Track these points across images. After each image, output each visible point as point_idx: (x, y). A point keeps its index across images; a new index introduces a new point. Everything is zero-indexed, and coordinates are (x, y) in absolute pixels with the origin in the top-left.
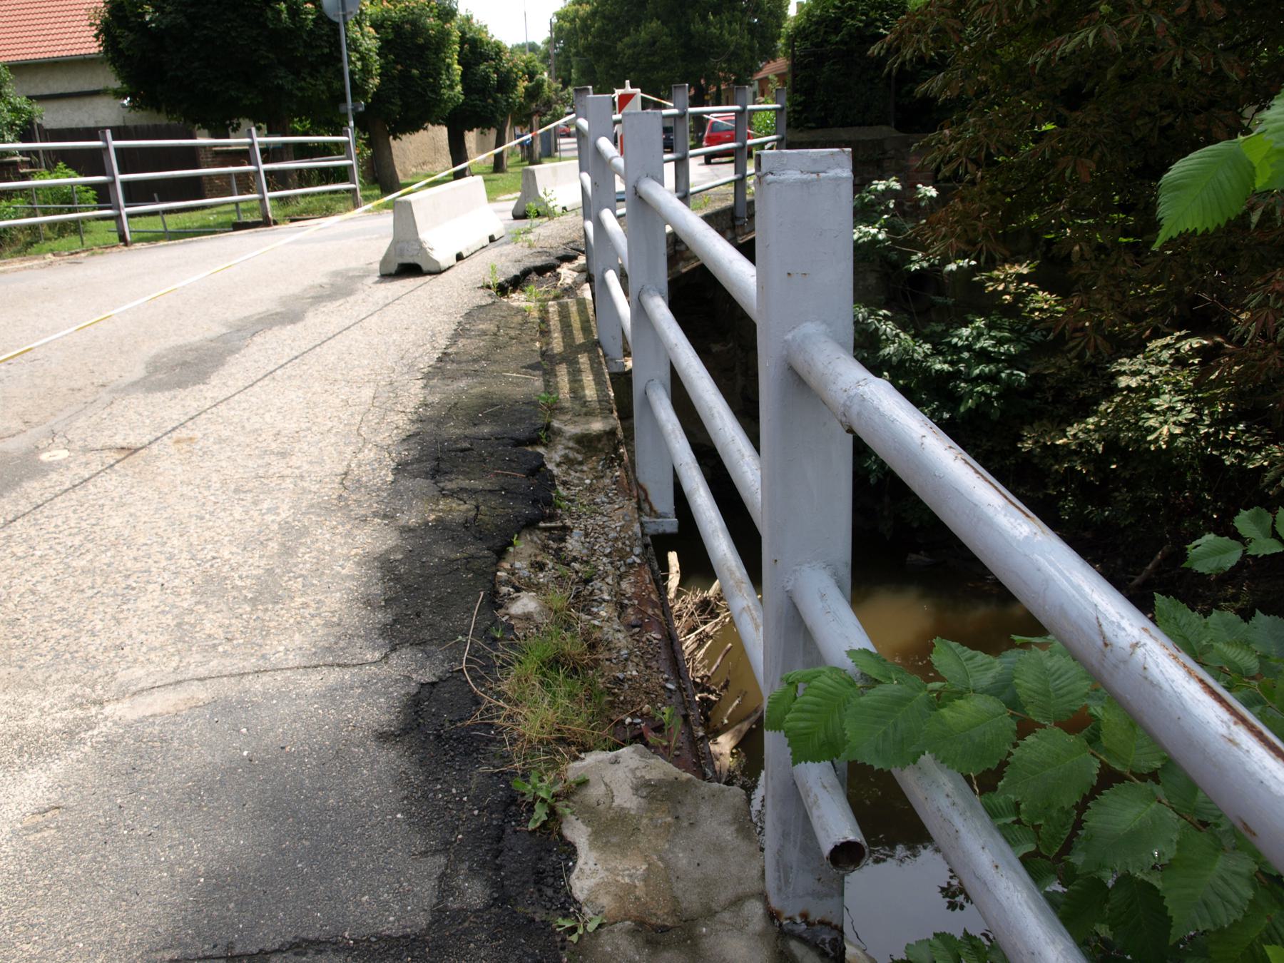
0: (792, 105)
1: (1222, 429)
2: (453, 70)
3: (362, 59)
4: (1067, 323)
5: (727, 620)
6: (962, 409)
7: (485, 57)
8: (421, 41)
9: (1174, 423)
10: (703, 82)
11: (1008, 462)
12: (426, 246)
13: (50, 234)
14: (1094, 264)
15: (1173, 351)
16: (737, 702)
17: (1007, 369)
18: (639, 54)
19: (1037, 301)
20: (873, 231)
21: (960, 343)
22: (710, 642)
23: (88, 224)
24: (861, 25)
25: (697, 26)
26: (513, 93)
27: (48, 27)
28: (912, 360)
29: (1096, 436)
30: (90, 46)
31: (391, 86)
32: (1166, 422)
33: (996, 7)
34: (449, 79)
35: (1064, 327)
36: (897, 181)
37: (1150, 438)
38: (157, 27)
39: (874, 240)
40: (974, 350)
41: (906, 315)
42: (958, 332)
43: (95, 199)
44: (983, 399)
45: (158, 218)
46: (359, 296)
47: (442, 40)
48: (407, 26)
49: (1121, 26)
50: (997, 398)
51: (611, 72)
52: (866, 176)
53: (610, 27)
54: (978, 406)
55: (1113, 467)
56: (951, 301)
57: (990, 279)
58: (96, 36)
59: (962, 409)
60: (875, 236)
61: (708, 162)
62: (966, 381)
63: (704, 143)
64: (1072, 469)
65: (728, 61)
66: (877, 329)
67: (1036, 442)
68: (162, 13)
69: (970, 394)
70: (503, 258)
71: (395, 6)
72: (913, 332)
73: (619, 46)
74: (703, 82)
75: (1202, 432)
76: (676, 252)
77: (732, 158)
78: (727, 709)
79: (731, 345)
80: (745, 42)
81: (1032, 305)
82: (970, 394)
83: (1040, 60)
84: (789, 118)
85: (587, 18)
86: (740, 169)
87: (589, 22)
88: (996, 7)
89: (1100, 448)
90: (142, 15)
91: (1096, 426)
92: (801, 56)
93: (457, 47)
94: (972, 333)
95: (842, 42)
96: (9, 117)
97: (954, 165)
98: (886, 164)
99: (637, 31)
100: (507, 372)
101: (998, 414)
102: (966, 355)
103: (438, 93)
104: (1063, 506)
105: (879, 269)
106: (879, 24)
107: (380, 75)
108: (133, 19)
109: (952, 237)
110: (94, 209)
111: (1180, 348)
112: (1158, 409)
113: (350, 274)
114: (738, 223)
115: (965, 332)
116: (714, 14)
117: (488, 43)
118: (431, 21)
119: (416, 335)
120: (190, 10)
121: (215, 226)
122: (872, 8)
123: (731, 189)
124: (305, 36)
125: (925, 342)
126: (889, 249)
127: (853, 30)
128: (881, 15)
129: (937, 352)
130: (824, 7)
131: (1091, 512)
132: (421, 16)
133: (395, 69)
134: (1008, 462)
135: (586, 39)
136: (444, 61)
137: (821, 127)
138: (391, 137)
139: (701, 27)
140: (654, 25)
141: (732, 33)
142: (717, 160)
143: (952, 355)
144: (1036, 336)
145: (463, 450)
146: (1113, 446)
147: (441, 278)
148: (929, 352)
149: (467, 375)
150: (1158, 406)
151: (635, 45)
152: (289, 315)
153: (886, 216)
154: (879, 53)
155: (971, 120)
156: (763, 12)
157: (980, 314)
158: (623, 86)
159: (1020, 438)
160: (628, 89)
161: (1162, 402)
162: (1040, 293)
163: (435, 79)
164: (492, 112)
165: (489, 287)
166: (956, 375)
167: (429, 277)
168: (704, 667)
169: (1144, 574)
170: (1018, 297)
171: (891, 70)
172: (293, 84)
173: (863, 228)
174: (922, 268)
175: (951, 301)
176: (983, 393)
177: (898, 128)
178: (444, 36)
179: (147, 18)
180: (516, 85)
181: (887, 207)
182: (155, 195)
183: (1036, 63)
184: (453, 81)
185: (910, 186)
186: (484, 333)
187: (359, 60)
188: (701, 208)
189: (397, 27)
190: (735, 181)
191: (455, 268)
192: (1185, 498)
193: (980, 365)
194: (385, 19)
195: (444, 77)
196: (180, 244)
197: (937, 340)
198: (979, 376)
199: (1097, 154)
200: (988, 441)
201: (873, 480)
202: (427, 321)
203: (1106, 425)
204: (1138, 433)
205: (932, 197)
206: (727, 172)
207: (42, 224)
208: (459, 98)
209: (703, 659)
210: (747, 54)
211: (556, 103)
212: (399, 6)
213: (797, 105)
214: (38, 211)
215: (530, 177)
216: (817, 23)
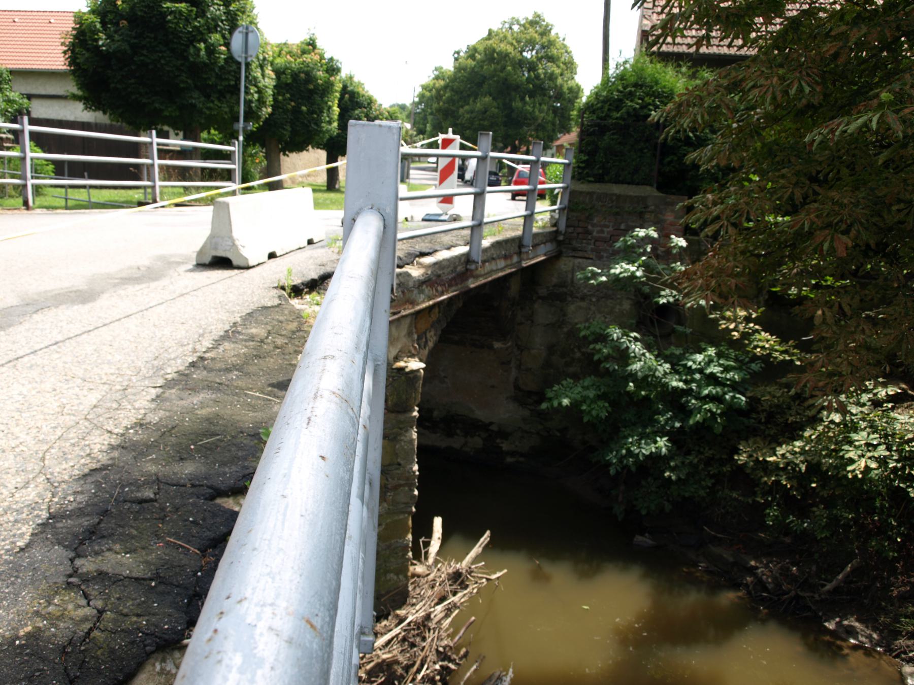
0: (577, 162)
1: (908, 465)
2: (333, 111)
3: (259, 92)
4: (808, 381)
5: (475, 591)
6: (691, 422)
8: (311, 87)
9: (870, 458)
10: (517, 142)
11: (724, 469)
12: (237, 243)
13: (13, 193)
14: (835, 328)
15: (870, 396)
16: (475, 667)
17: (730, 392)
18: (475, 118)
19: (760, 340)
20: (633, 269)
21: (694, 367)
22: (457, 611)
23: (44, 189)
24: (638, 106)
25: (517, 104)
27: (52, 48)
28: (653, 376)
29: (802, 458)
30: (57, 61)
31: (285, 116)
32: (863, 456)
33: (771, 89)
34: (328, 117)
35: (805, 386)
36: (655, 231)
37: (849, 468)
38: (107, 50)
39: (633, 276)
40: (705, 374)
41: (651, 338)
42: (693, 357)
43: (53, 172)
44: (709, 415)
45: (63, 190)
46: (164, 282)
47: (327, 88)
48: (302, 75)
49: (902, 114)
50: (721, 415)
52: (631, 224)
53: (456, 98)
54: (704, 420)
55: (814, 485)
56: (689, 331)
57: (724, 318)
58: (65, 52)
59: (691, 422)
60: (633, 273)
61: (513, 199)
62: (696, 399)
64: (777, 482)
65: (537, 130)
66: (628, 348)
67: (750, 456)
68: (113, 40)
69: (699, 410)
70: (312, 261)
72: (656, 353)
73: (461, 111)
74: (517, 142)
75: (891, 466)
76: (467, 270)
77: (525, 198)
78: (465, 674)
79: (509, 344)
80: (550, 118)
81: (755, 343)
82: (699, 410)
83: (818, 139)
84: (574, 172)
86: (530, 207)
87: (442, 92)
88: (771, 89)
89: (803, 468)
90: (97, 40)
91: (802, 449)
92: (588, 126)
93: (338, 95)
94: (704, 359)
95: (622, 118)
96: (3, 105)
97: (715, 227)
98: (647, 216)
99: (474, 101)
100: (251, 389)
101: (721, 429)
102: (697, 376)
104: (769, 513)
105: (633, 298)
106: (651, 107)
107: (272, 106)
108: (90, 42)
109: (707, 290)
110: (51, 178)
111: (877, 393)
112: (857, 443)
113: (172, 259)
114: (523, 250)
115: (699, 357)
116: (530, 97)
117: (363, 96)
119: (187, 331)
120: (133, 41)
121: (123, 202)
122: (647, 95)
123: (522, 221)
124: (217, 70)
125: (666, 362)
126: (643, 283)
127: (631, 110)
128: (654, 101)
129: (674, 371)
130: (610, 90)
131: (792, 521)
133: (289, 104)
134: (724, 469)
135: (439, 104)
136: (327, 103)
137: (599, 182)
141: (541, 111)
142: (520, 198)
143: (686, 375)
144: (755, 367)
145: (142, 501)
146: (814, 468)
147: (246, 273)
148: (668, 371)
149: (209, 388)
150: (857, 441)
151: (472, 112)
152: (84, 296)
153: (644, 258)
154: (659, 120)
155: (732, 189)
156: (564, 99)
157: (713, 343)
158: (446, 133)
159: (737, 451)
160: (450, 135)
161: (861, 437)
162: (763, 333)
163: (318, 115)
165: (283, 288)
166: (688, 392)
167: (236, 271)
168: (448, 636)
169: (834, 582)
170: (745, 335)
171: (667, 135)
172: (204, 104)
173: (624, 265)
174: (668, 302)
175: (689, 331)
176: (710, 411)
177: (659, 188)
179: (101, 43)
181: (645, 250)
182: (86, 174)
183: (814, 141)
184: (331, 119)
185: (665, 235)
186: (252, 338)
187: (256, 92)
188: (494, 235)
189: (295, 75)
190: (525, 217)
191: (265, 265)
192: (873, 520)
193: (708, 385)
194: (287, 68)
195: (325, 115)
196: (71, 214)
197: (675, 361)
198: (707, 396)
199: (853, 232)
200: (710, 449)
201: (612, 471)
202: (207, 318)
203: (810, 450)
204: (838, 461)
205: (682, 247)
206: (520, 208)
207: (9, 184)
209: (447, 630)
210: (550, 127)
212: (298, 60)
213: (581, 162)
214: (7, 175)
216: (604, 102)
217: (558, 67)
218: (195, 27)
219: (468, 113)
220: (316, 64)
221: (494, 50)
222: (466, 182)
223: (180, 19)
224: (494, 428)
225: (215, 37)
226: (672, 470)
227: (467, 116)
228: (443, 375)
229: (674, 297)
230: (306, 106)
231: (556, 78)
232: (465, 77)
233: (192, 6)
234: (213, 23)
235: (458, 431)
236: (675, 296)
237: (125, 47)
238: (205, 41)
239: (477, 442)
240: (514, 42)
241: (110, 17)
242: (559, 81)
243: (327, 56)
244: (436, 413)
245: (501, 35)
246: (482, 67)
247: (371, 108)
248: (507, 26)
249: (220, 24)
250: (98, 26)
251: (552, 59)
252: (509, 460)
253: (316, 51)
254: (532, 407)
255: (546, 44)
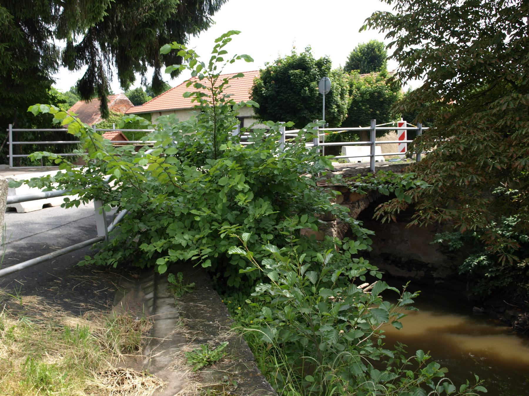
8: (381, 99)
48: (376, 94)
63: (512, 30)
90: (261, 91)
120: (277, 90)
189: (372, 94)
224: (430, 266)
225: (313, 84)
226: (490, 272)
228: (406, 239)
230: (379, 111)
235: (414, 268)
237: (274, 93)
239: (422, 273)
241: (268, 79)
244: (403, 259)
250: (263, 84)
252: (437, 282)
254: (448, 254)
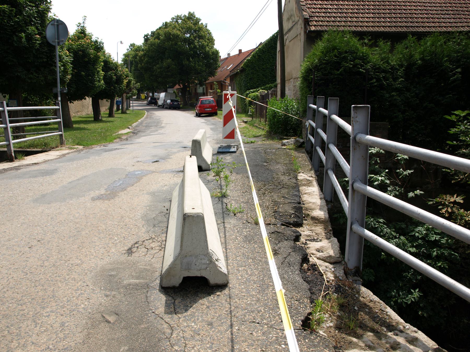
7: (111, 69)
8: (87, 60)
25: (186, 62)
26: (122, 84)
51: (151, 78)
71: (75, 43)
80: (204, 69)
85: (142, 57)
95: (341, 74)
103: (93, 84)
107: (72, 74)
117: (112, 63)
118: (92, 51)
124: (34, 51)
132: (87, 48)
136: (96, 69)
138: (69, 102)
139: (187, 62)
140: (169, 61)
141: (199, 65)
163: (92, 77)
164: (113, 92)
178: (97, 58)
180: (123, 82)
184: (100, 78)
195: (96, 76)
208: (103, 86)
211: (133, 89)
212: (77, 43)
215: (198, 145)
217: (205, 41)
218: (16, 22)
219: (159, 69)
220: (88, 45)
221: (170, 34)
222: (159, 106)
223: (4, 16)
225: (32, 29)
227: (159, 70)
229: (398, 191)
231: (205, 47)
232: (155, 49)
233: (12, 7)
234: (28, 19)
236: (399, 190)
238: (25, 32)
240: (180, 29)
242: (207, 49)
243: (94, 39)
245: (173, 26)
246: (164, 43)
247: (117, 70)
248: (175, 20)
249: (33, 19)
251: (201, 37)
253: (87, 37)
255: (198, 29)
